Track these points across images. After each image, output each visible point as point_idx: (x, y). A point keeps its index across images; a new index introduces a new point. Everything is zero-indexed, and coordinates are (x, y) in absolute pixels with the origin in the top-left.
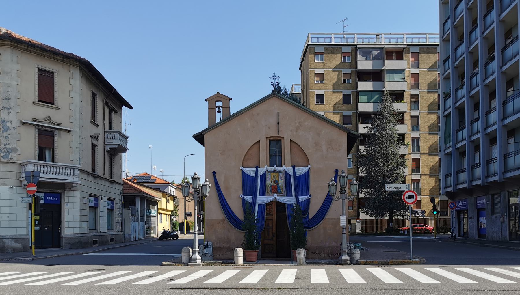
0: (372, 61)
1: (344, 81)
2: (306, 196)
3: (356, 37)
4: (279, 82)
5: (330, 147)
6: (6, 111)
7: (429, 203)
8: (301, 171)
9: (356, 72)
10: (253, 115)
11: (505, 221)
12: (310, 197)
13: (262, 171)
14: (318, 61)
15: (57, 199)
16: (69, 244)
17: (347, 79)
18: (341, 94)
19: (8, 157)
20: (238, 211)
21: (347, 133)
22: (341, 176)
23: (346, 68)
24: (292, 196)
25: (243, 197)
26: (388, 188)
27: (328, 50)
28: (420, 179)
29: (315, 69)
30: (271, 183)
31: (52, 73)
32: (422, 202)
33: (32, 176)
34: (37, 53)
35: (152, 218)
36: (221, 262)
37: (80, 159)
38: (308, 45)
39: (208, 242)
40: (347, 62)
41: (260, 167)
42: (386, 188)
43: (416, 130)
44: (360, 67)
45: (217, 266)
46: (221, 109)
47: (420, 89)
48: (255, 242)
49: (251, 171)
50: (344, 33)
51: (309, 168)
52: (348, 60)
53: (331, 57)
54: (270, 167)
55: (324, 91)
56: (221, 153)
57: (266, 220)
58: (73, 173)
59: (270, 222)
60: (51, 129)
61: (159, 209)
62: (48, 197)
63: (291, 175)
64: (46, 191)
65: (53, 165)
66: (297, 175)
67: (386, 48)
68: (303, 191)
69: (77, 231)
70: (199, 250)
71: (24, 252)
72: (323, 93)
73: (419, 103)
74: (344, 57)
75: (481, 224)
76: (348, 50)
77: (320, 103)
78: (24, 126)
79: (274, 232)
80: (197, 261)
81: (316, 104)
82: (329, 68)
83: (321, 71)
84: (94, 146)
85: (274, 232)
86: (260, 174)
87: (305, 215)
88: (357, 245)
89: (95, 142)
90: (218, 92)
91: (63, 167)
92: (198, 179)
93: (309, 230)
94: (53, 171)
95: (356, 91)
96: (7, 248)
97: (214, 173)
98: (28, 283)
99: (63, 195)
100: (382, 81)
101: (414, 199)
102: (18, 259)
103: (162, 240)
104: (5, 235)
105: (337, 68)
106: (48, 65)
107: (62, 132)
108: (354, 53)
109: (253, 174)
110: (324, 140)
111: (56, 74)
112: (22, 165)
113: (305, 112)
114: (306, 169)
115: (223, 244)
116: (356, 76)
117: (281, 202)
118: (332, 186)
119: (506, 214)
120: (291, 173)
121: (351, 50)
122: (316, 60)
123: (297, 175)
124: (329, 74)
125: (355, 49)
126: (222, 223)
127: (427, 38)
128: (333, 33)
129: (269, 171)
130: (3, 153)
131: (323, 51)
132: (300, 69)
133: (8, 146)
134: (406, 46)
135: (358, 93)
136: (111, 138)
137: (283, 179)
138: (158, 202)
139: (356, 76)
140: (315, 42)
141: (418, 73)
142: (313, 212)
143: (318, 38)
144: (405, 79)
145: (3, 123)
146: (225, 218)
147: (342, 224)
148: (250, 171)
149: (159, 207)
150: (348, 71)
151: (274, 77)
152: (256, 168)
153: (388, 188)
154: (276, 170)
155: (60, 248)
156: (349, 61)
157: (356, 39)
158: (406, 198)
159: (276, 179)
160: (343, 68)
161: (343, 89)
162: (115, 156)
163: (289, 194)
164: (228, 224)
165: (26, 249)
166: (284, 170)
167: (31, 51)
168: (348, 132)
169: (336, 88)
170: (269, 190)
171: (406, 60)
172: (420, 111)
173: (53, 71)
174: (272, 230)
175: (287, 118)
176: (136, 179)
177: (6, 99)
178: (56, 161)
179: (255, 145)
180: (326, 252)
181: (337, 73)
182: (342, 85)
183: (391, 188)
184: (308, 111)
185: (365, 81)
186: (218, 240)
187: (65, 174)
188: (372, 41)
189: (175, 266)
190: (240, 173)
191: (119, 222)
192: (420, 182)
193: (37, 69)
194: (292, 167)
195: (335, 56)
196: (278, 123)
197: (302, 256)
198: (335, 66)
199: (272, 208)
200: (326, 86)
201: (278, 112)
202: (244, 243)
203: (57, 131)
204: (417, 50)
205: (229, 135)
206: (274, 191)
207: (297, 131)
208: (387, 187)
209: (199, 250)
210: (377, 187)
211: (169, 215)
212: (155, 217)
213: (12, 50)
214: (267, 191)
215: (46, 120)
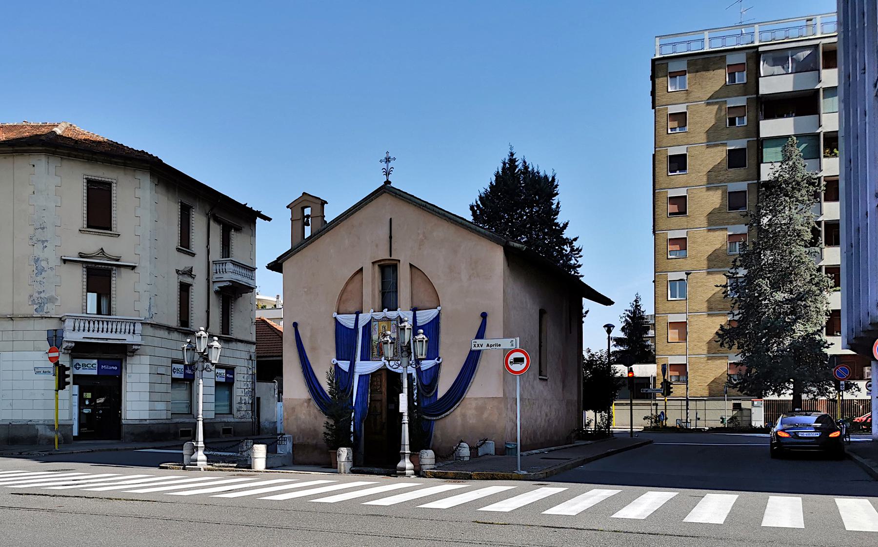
0: (792, 75)
1: (732, 122)
4: (514, 151)
6: (40, 245)
8: (425, 316)
10: (353, 226)
12: (438, 362)
13: (364, 319)
14: (676, 88)
15: (116, 368)
16: (132, 434)
17: (737, 119)
18: (725, 148)
19: (42, 311)
23: (736, 96)
25: (337, 363)
26: (476, 346)
30: (379, 338)
31: (109, 184)
33: (54, 337)
34: (85, 158)
36: (235, 465)
37: (150, 308)
40: (736, 83)
41: (362, 313)
50: (741, 25)
51: (439, 311)
52: (741, 79)
56: (305, 292)
58: (134, 330)
60: (106, 267)
62: (102, 366)
64: (98, 357)
65: (108, 320)
69: (145, 415)
70: (410, 452)
71: (64, 443)
72: (686, 151)
74: (732, 76)
76: (741, 58)
78: (66, 264)
79: (384, 421)
80: (198, 463)
81: (670, 174)
82: (697, 100)
84: (185, 289)
87: (429, 393)
88: (508, 446)
89: (188, 280)
91: (122, 321)
92: (202, 338)
93: (437, 418)
94: (99, 327)
96: (40, 438)
98: (127, 490)
99: (124, 361)
100: (816, 114)
101: (524, 365)
102: (31, 453)
104: (38, 421)
105: (716, 98)
106: (101, 173)
107: (122, 269)
108: (752, 65)
109: (351, 325)
111: (115, 185)
112: (62, 321)
114: (433, 313)
115: (308, 439)
121: (747, 59)
122: (671, 86)
124: (697, 113)
125: (755, 55)
130: (37, 304)
131: (686, 66)
133: (42, 295)
135: (761, 143)
136: (221, 270)
140: (668, 52)
142: (443, 387)
143: (674, 44)
145: (37, 262)
146: (310, 397)
148: (348, 321)
150: (741, 101)
152: (355, 315)
153: (476, 346)
154: (386, 317)
155: (120, 440)
156: (743, 81)
157: (757, 35)
158: (510, 362)
161: (727, 139)
162: (236, 299)
164: (314, 408)
165: (67, 439)
167: (76, 157)
169: (713, 137)
173: (110, 180)
177: (41, 228)
178: (114, 313)
181: (717, 107)
182: (727, 131)
183: (482, 346)
184: (436, 212)
185: (781, 116)
187: (121, 331)
189: (171, 469)
191: (245, 403)
193: (85, 181)
195: (710, 74)
196: (391, 237)
197: (342, 461)
199: (381, 381)
200: (692, 137)
201: (391, 219)
203: (114, 268)
208: (475, 345)
209: (410, 452)
210: (760, 334)
213: (48, 158)
215: (98, 254)
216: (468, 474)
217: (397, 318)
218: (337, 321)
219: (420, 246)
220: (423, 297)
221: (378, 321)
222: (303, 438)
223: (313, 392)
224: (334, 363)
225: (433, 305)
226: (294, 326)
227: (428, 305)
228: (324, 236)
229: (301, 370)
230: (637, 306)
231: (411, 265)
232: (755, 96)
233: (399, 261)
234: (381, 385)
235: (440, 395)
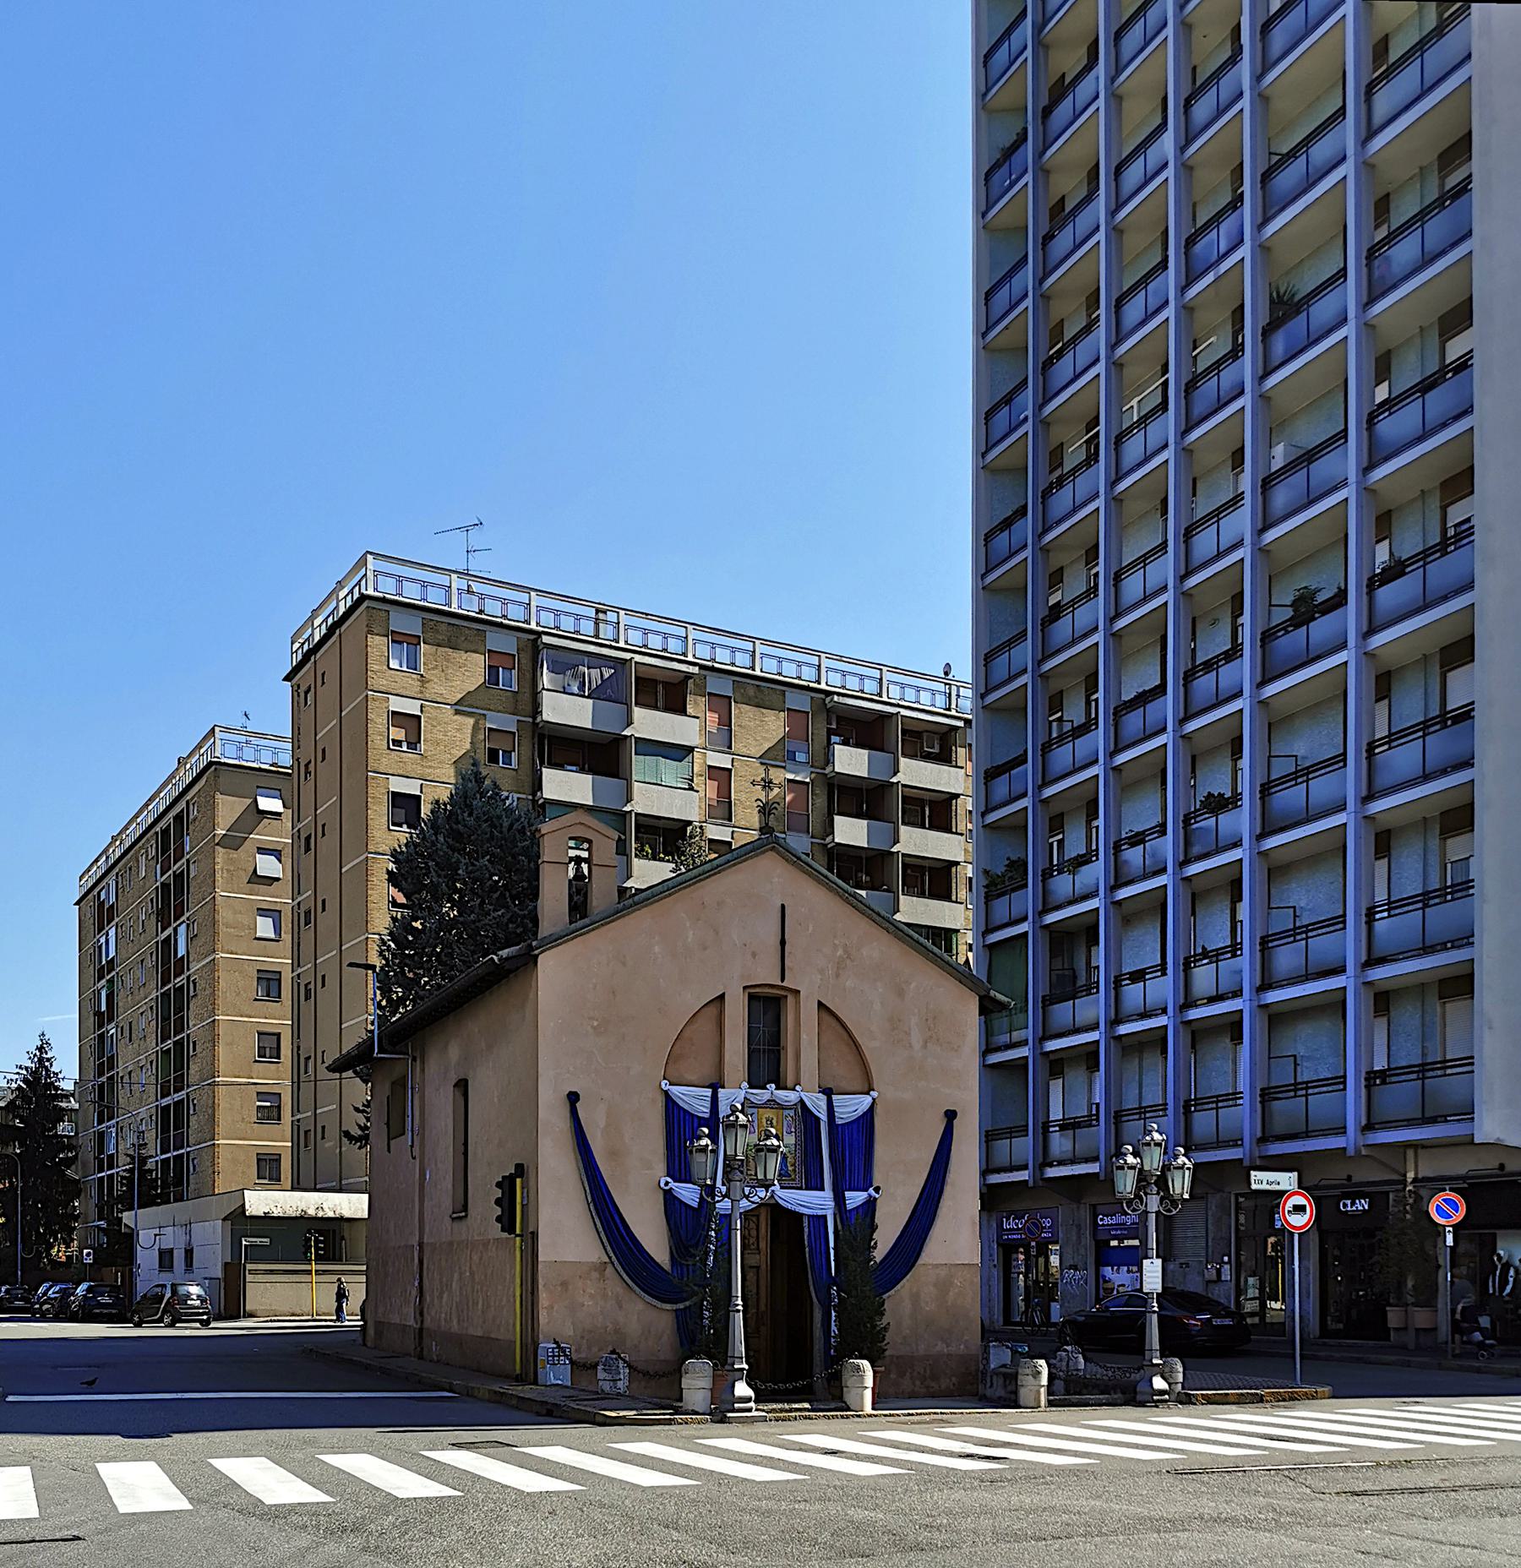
3: (454, 586)
5: (931, 1037)
8: (850, 1107)
9: (534, 732)
11: (1223, 1278)
17: (501, 752)
20: (653, 1238)
22: (1152, 1143)
24: (822, 1189)
27: (437, 631)
29: (390, 696)
38: (363, 598)
40: (501, 686)
41: (723, 1087)
42: (1253, 1182)
44: (548, 715)
47: (737, 824)
49: (700, 1098)
53: (448, 661)
55: (422, 785)
66: (839, 1122)
74: (492, 670)
75: (1109, 1285)
76: (506, 644)
77: (405, 826)
79: (763, 1308)
81: (392, 828)
82: (438, 699)
83: (412, 707)
95: (534, 801)
100: (615, 775)
101: (1307, 1217)
110: (916, 1011)
116: (534, 744)
119: (1226, 1259)
125: (533, 645)
126: (595, 1275)
128: (536, 590)
132: (287, 678)
134: (696, 670)
139: (534, 744)
140: (388, 588)
143: (400, 579)
144: (692, 780)
147: (1148, 1286)
148: (695, 1099)
150: (509, 723)
158: (1289, 1212)
160: (489, 710)
163: (816, 1184)
164: (615, 1283)
168: (984, 993)
171: (698, 718)
179: (706, 1009)
181: (471, 721)
189: (681, 1424)
195: (460, 656)
196: (783, 943)
198: (460, 696)
200: (430, 767)
201: (783, 906)
204: (724, 687)
205: (624, 964)
207: (838, 976)
216: (1257, 1394)
218: (669, 1102)
220: (844, 1072)
222: (589, 1348)
225: (858, 1087)
230: (41, 1060)
231: (820, 1004)
232: (530, 720)
235: (879, 1254)
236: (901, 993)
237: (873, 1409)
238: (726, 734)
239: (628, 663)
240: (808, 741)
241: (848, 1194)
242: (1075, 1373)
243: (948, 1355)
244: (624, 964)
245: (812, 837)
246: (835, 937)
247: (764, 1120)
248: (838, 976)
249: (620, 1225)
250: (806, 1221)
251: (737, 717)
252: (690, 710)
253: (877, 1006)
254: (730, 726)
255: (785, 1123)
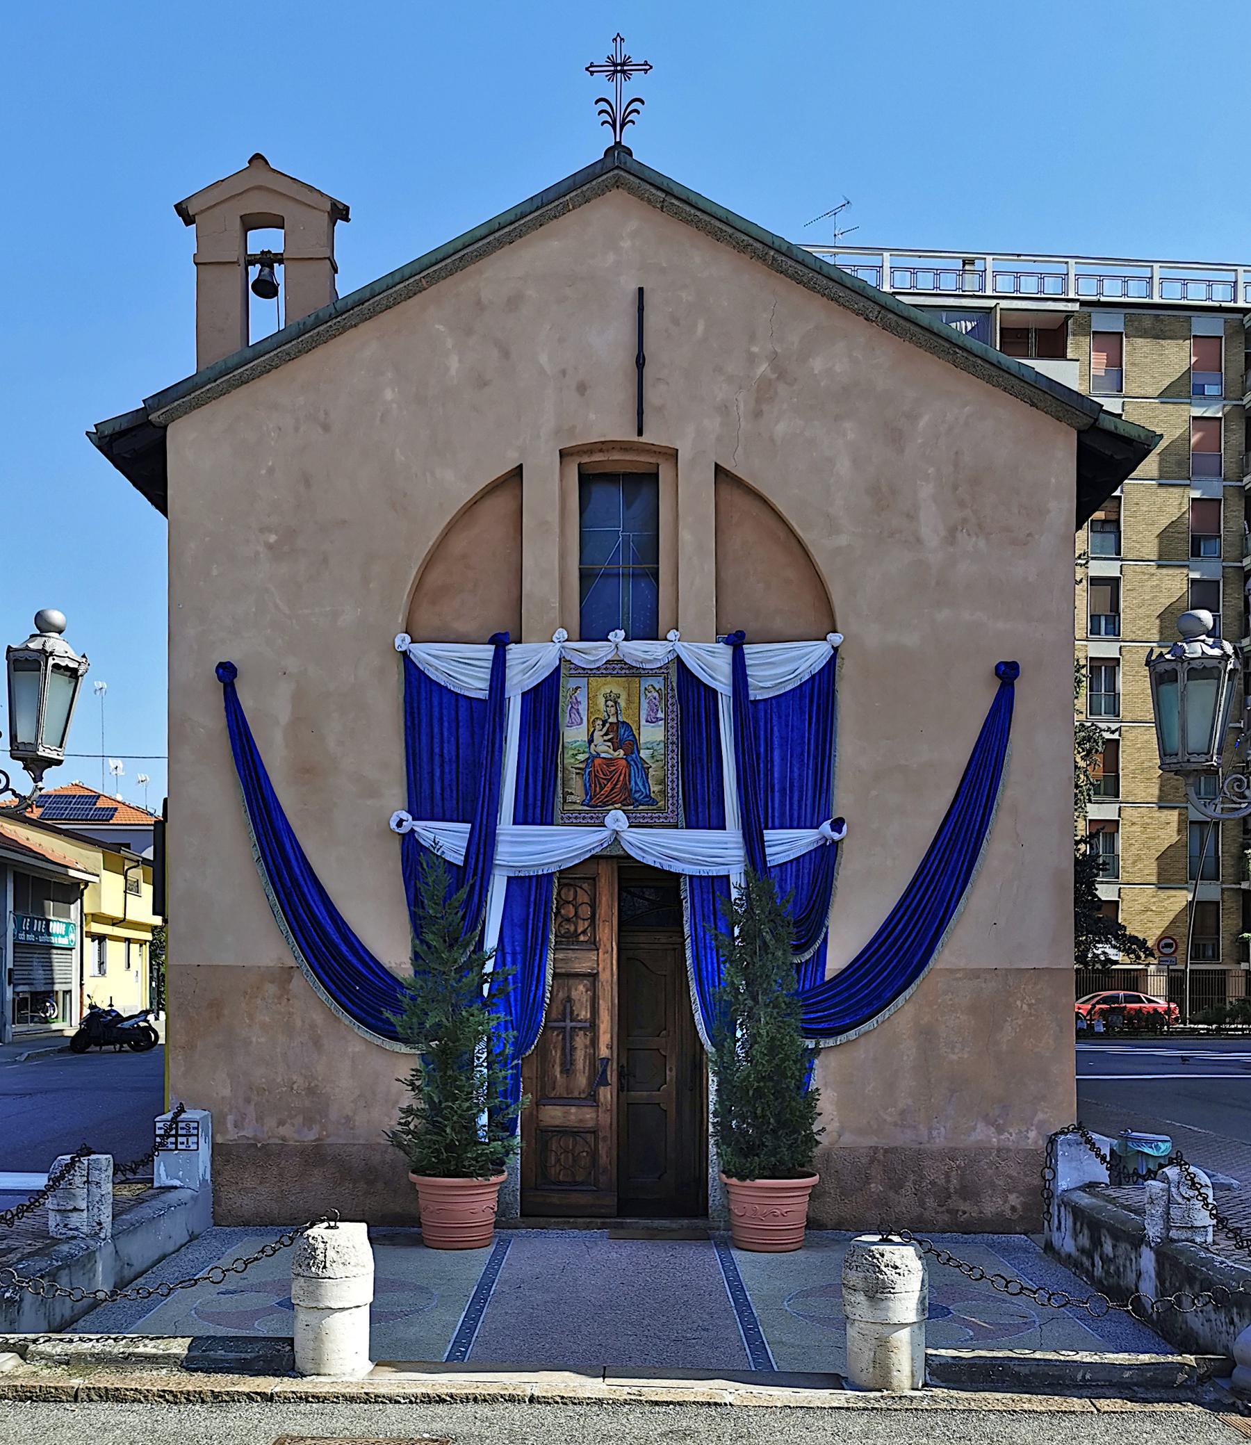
2: (812, 827)
3: (887, 265)
7: (1149, 913)
10: (479, 303)
12: (836, 836)
21: (1079, 432)
24: (722, 826)
25: (412, 831)
28: (1118, 821)
30: (591, 741)
32: (1125, 908)
35: (56, 957)
39: (181, 1110)
41: (520, 642)
43: (1106, 634)
45: (124, 1400)
46: (279, 269)
48: (484, 1119)
51: (836, 649)
54: (581, 640)
56: (270, 547)
57: (555, 976)
59: (581, 988)
61: (89, 918)
63: (715, 692)
66: (755, 695)
67: (1001, 309)
68: (796, 798)
73: (1122, 529)
79: (604, 1052)
85: (604, 1052)
86: (519, 681)
88: (1147, 1150)
90: (258, 157)
97: (227, 672)
103: (82, 1051)
113: (813, 289)
114: (813, 655)
115: (281, 1123)
117: (649, 860)
118: (1192, 684)
120: (722, 683)
123: (755, 695)
126: (271, 989)
127: (1156, 281)
129: (577, 667)
134: (1076, 307)
137: (665, 719)
138: (82, 887)
141: (1120, 412)
146: (291, 962)
149: (85, 911)
151: (620, 68)
152: (493, 647)
159: (620, 719)
166: (671, 657)
170: (577, 786)
171: (1078, 360)
172: (1122, 560)
174: (594, 1042)
175: (701, 328)
176: (37, 807)
179: (488, 504)
180: (933, 1183)
186: (248, 1101)
188: (948, 283)
190: (395, 678)
192: (1118, 832)
194: (727, 642)
196: (640, 362)
201: (641, 290)
202: (412, 1127)
204: (1114, 322)
205: (326, 428)
206: (607, 789)
207: (758, 414)
211: (141, 943)
212: (71, 949)
214: (565, 794)
217: (666, 666)
218: (414, 677)
219: (758, 401)
221: (586, 673)
223: (976, 844)
224: (404, 830)
226: (220, 679)
227: (778, 624)
228: (353, 331)
229: (257, 853)
231: (720, 472)
233: (673, 455)
234: (593, 917)
236: (896, 437)
237: (382, 1355)
238: (1115, 376)
239: (993, 311)
240: (1221, 371)
241: (769, 835)
242: (1184, 1235)
243: (999, 1150)
244: (326, 428)
245: (1225, 480)
246: (752, 338)
247: (601, 700)
248: (758, 414)
249: (892, 926)
250: (685, 888)
251: (1128, 354)
252: (1069, 356)
253: (844, 467)
254: (1121, 366)
255: (644, 705)
